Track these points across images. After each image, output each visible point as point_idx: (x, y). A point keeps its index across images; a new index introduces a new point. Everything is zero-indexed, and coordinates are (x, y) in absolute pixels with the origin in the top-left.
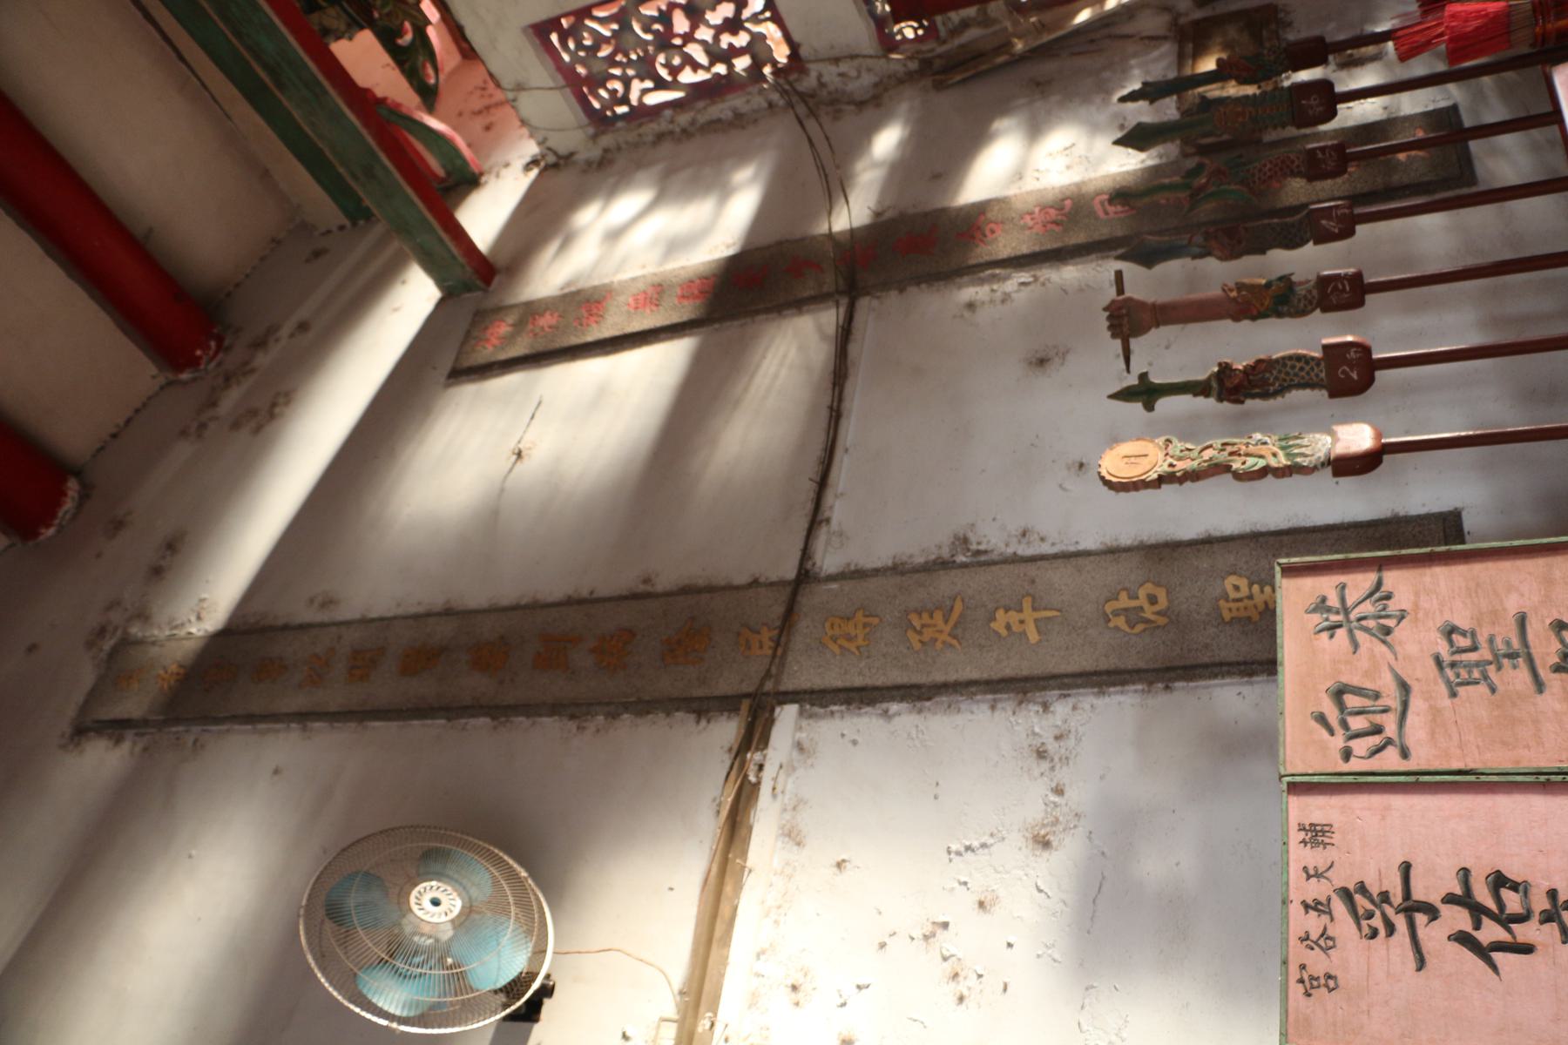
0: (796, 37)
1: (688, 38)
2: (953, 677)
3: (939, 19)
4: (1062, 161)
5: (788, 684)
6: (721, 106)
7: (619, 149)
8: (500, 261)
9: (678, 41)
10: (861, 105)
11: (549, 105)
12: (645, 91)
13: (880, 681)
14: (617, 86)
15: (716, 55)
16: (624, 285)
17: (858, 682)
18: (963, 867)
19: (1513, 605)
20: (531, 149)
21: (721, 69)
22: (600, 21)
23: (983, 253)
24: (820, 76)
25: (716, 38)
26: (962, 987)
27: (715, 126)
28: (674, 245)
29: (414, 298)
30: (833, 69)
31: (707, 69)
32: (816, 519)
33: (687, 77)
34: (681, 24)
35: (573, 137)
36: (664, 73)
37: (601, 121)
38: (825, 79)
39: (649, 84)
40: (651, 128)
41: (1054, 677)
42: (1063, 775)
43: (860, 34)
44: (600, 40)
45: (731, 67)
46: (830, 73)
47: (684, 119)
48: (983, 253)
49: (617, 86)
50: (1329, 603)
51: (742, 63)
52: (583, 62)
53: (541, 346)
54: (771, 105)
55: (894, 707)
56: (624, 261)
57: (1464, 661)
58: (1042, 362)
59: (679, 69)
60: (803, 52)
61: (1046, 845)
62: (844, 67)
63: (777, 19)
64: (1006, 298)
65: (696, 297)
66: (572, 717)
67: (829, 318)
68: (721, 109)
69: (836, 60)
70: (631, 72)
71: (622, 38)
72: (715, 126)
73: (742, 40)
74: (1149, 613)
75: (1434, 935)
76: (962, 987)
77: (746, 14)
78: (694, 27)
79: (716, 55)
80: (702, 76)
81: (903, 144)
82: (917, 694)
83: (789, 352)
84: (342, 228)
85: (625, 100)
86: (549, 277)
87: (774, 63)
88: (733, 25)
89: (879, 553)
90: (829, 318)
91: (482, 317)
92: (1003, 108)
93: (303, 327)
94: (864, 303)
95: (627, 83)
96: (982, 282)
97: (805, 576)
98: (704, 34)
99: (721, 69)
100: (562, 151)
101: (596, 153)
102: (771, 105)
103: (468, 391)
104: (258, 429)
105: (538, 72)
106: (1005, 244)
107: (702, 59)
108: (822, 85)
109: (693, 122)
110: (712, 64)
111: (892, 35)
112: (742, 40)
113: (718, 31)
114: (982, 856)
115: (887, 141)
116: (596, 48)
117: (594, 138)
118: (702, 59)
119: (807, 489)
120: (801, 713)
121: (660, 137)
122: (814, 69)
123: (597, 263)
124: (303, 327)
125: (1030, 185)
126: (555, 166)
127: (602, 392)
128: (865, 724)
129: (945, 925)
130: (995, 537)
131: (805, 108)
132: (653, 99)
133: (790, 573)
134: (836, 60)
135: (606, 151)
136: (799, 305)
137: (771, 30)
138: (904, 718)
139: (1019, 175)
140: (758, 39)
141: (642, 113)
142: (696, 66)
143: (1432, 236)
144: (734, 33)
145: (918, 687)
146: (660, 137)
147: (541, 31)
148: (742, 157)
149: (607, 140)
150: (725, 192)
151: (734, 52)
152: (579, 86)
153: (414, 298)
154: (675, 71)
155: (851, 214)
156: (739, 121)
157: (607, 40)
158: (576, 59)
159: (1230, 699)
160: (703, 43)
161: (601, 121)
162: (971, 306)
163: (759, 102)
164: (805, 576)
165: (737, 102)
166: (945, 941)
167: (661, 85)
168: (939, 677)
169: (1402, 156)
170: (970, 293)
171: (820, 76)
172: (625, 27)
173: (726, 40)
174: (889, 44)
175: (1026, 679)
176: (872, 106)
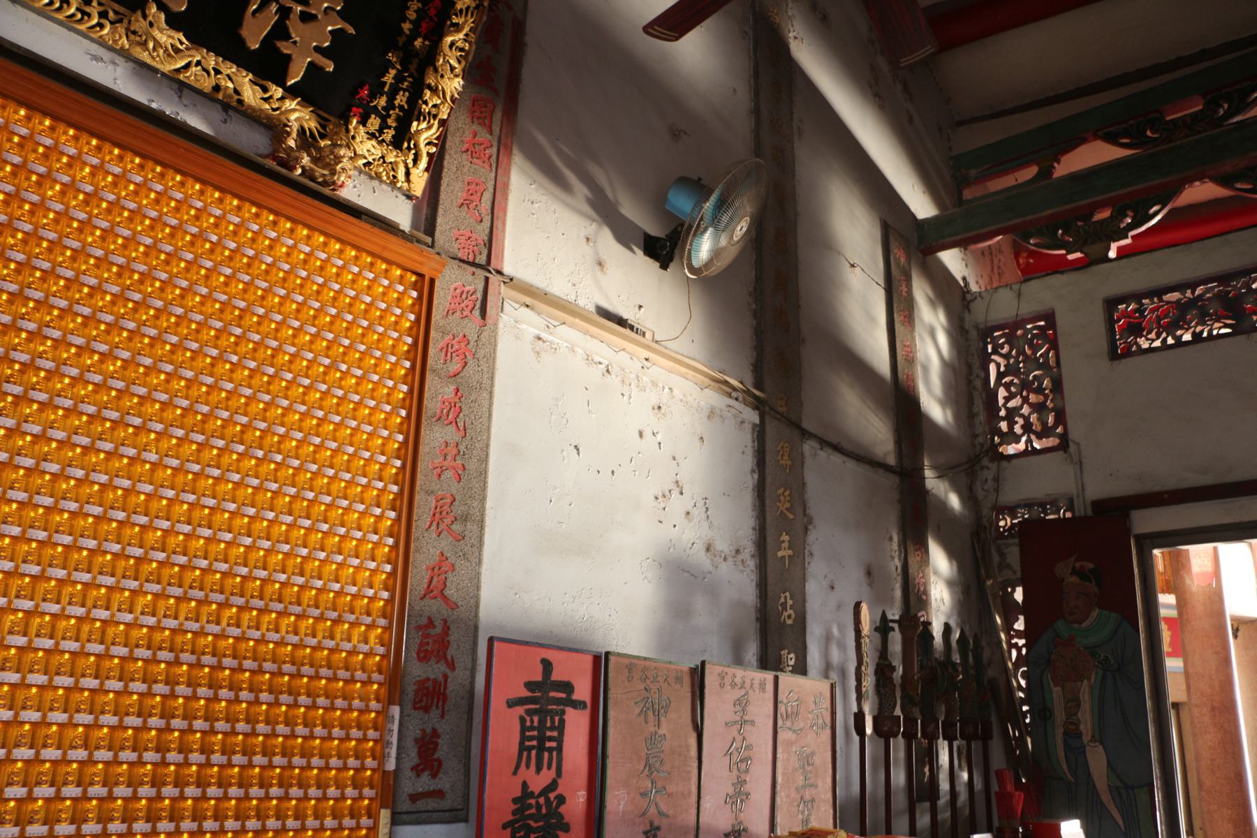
0: (1014, 461)
1: (1025, 400)
2: (768, 509)
3: (1017, 541)
4: (938, 597)
5: (768, 420)
6: (981, 407)
7: (967, 340)
8: (929, 258)
9: (1024, 393)
10: (970, 488)
11: (1004, 306)
12: (998, 365)
13: (768, 471)
14: (1005, 350)
15: (1012, 414)
16: (913, 339)
17: (768, 458)
18: (700, 504)
19: (820, 783)
20: (974, 288)
21: (1003, 413)
22: (1047, 352)
23: (911, 548)
24: (988, 468)
25: (1022, 416)
26: (661, 499)
27: (971, 401)
28: (926, 369)
29: (922, 206)
30: (990, 477)
31: (1004, 405)
32: (824, 443)
33: (1002, 393)
34: (1033, 398)
35: (979, 314)
36: (1007, 379)
37: (986, 333)
38: (985, 471)
39: (1002, 369)
40: (976, 363)
41: (765, 563)
42: (730, 559)
43: (1010, 495)
44: (1035, 349)
45: (1003, 419)
46: (989, 475)
47: (978, 384)
48: (911, 548)
49: (1005, 350)
50: (576, 696)
51: (1004, 425)
52: (1025, 335)
53: (895, 284)
54: (976, 436)
55: (756, 476)
56: (922, 339)
57: (807, 760)
58: (869, 573)
59: (1008, 390)
60: (1004, 463)
61: (708, 550)
62: (990, 483)
63: (1025, 453)
64: (893, 558)
65: (500, 167)
66: (755, 289)
67: (891, 460)
68: (979, 406)
69: (996, 479)
70: (1012, 361)
71: (1032, 361)
72: (971, 401)
73: (1018, 429)
74: (786, 614)
75: (734, 731)
76: (661, 499)
77: (1033, 437)
78: (1031, 405)
79: (1012, 414)
80: (1001, 401)
81: (952, 510)
82: (760, 490)
83: (876, 431)
84: (950, 149)
85: (995, 352)
86: (921, 292)
87: (1000, 444)
88: (1027, 428)
89: (811, 478)
90: (891, 460)
91: (907, 245)
92: (961, 568)
93: (910, 119)
94: (895, 480)
95: (1005, 356)
96: (899, 546)
97: (805, 434)
98: (1026, 410)
99: (1003, 413)
100: (972, 305)
101: (967, 325)
102: (976, 436)
103: (878, 234)
104: (870, 85)
105: (1027, 309)
106: (913, 560)
107: (1010, 405)
108: (982, 468)
109: (974, 388)
110: (1007, 409)
111: (1003, 514)
112: (1018, 429)
113: (1026, 419)
114: (703, 516)
115: (954, 501)
116: (1031, 346)
117: (976, 327)
118: (1010, 405)
119: (835, 440)
120: (755, 425)
121: (969, 366)
122: (994, 466)
123: (922, 321)
124: (910, 119)
125: (933, 578)
126: (964, 298)
127: (872, 320)
128: (749, 461)
129: (681, 493)
130: (812, 537)
131: (976, 457)
132: (992, 368)
133: (805, 425)
134: (996, 479)
135: (967, 332)
136: (898, 443)
137: (1021, 446)
138: (750, 481)
139: (936, 573)
140: (1017, 439)
141: (986, 360)
142: (1007, 399)
143: (899, 777)
144: (1022, 427)
145: (764, 490)
146: (969, 366)
147: (1050, 317)
148: (957, 415)
149: (973, 334)
150: (943, 404)
151: (1011, 424)
152: (1012, 327)
153: (922, 206)
154: (1007, 386)
155: (933, 482)
156: (971, 416)
157: (1035, 353)
158: (1027, 331)
159: (752, 651)
160: (1021, 407)
161: (986, 333)
162: (891, 539)
163: (979, 429)
164: (805, 434)
165: (982, 417)
166: (675, 493)
167: (1000, 376)
168: (767, 502)
169: (927, 769)
170: (895, 538)
171: (988, 468)
172: (1040, 367)
173: (1021, 421)
174: (1002, 510)
175: (765, 548)
176: (969, 497)
